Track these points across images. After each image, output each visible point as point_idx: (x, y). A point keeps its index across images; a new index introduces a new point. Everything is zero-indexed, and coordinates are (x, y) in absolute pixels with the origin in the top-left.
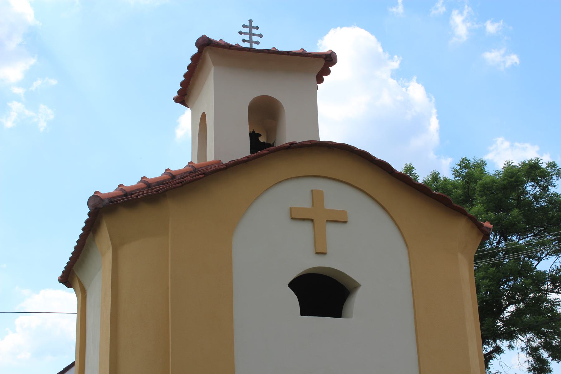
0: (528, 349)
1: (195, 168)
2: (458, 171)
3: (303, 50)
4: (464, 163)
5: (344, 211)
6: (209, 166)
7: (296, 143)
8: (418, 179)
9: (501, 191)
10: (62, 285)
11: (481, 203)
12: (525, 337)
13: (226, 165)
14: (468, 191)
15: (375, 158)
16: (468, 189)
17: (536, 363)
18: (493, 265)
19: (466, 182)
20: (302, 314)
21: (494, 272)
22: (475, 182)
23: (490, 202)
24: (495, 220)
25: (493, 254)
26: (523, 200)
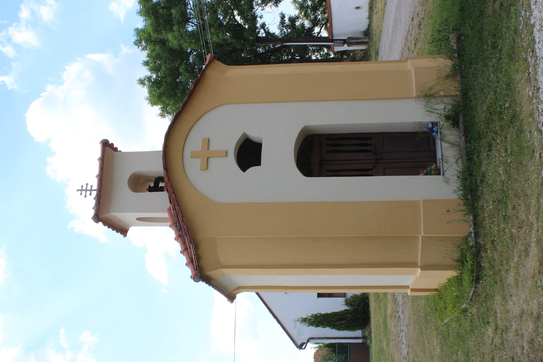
3: (99, 159)
4: (137, 44)
8: (147, 76)
10: (235, 301)
11: (166, 35)
12: (255, 7)
14: (157, 42)
20: (260, 165)
21: (214, 29)
23: (166, 28)
24: (179, 25)
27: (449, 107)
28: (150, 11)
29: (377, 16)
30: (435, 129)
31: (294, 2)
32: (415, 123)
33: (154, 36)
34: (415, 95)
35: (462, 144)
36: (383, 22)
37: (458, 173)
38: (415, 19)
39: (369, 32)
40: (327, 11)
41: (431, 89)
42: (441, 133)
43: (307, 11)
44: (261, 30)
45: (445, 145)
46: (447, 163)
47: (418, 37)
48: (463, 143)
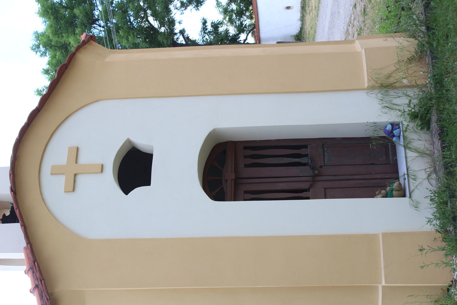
0: (182, 10)
1: (30, 269)
2: (41, 54)
4: (35, 49)
5: (69, 149)
6: (28, 257)
7: (11, 186)
9: (59, 21)
11: (68, 38)
13: (28, 244)
14: (58, 47)
15: (26, 123)
16: (56, 46)
17: (193, 4)
18: (117, 31)
19: (51, 47)
20: (150, 185)
21: (123, 31)
22: (51, 41)
23: (68, 31)
24: (82, 28)
25: (109, 31)
26: (66, 4)
27: (415, 101)
28: (49, 10)
29: (310, 16)
30: (395, 132)
31: (218, 7)
32: (367, 124)
33: (54, 39)
34: (366, 85)
35: (436, 152)
36: (318, 21)
37: (431, 193)
38: (358, 5)
39: (302, 36)
40: (254, 16)
41: (389, 76)
42: (405, 138)
43: (232, 16)
44: (179, 37)
45: (411, 154)
46: (415, 179)
47: (362, 26)
48: (438, 150)
